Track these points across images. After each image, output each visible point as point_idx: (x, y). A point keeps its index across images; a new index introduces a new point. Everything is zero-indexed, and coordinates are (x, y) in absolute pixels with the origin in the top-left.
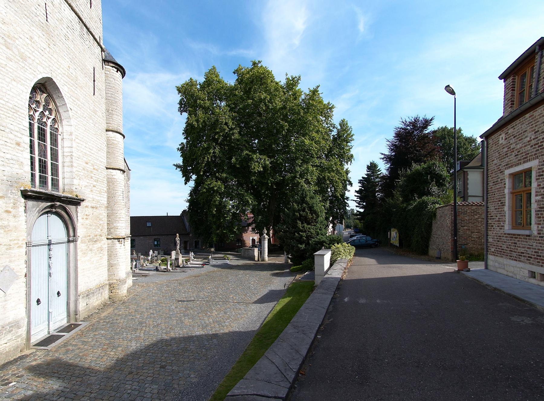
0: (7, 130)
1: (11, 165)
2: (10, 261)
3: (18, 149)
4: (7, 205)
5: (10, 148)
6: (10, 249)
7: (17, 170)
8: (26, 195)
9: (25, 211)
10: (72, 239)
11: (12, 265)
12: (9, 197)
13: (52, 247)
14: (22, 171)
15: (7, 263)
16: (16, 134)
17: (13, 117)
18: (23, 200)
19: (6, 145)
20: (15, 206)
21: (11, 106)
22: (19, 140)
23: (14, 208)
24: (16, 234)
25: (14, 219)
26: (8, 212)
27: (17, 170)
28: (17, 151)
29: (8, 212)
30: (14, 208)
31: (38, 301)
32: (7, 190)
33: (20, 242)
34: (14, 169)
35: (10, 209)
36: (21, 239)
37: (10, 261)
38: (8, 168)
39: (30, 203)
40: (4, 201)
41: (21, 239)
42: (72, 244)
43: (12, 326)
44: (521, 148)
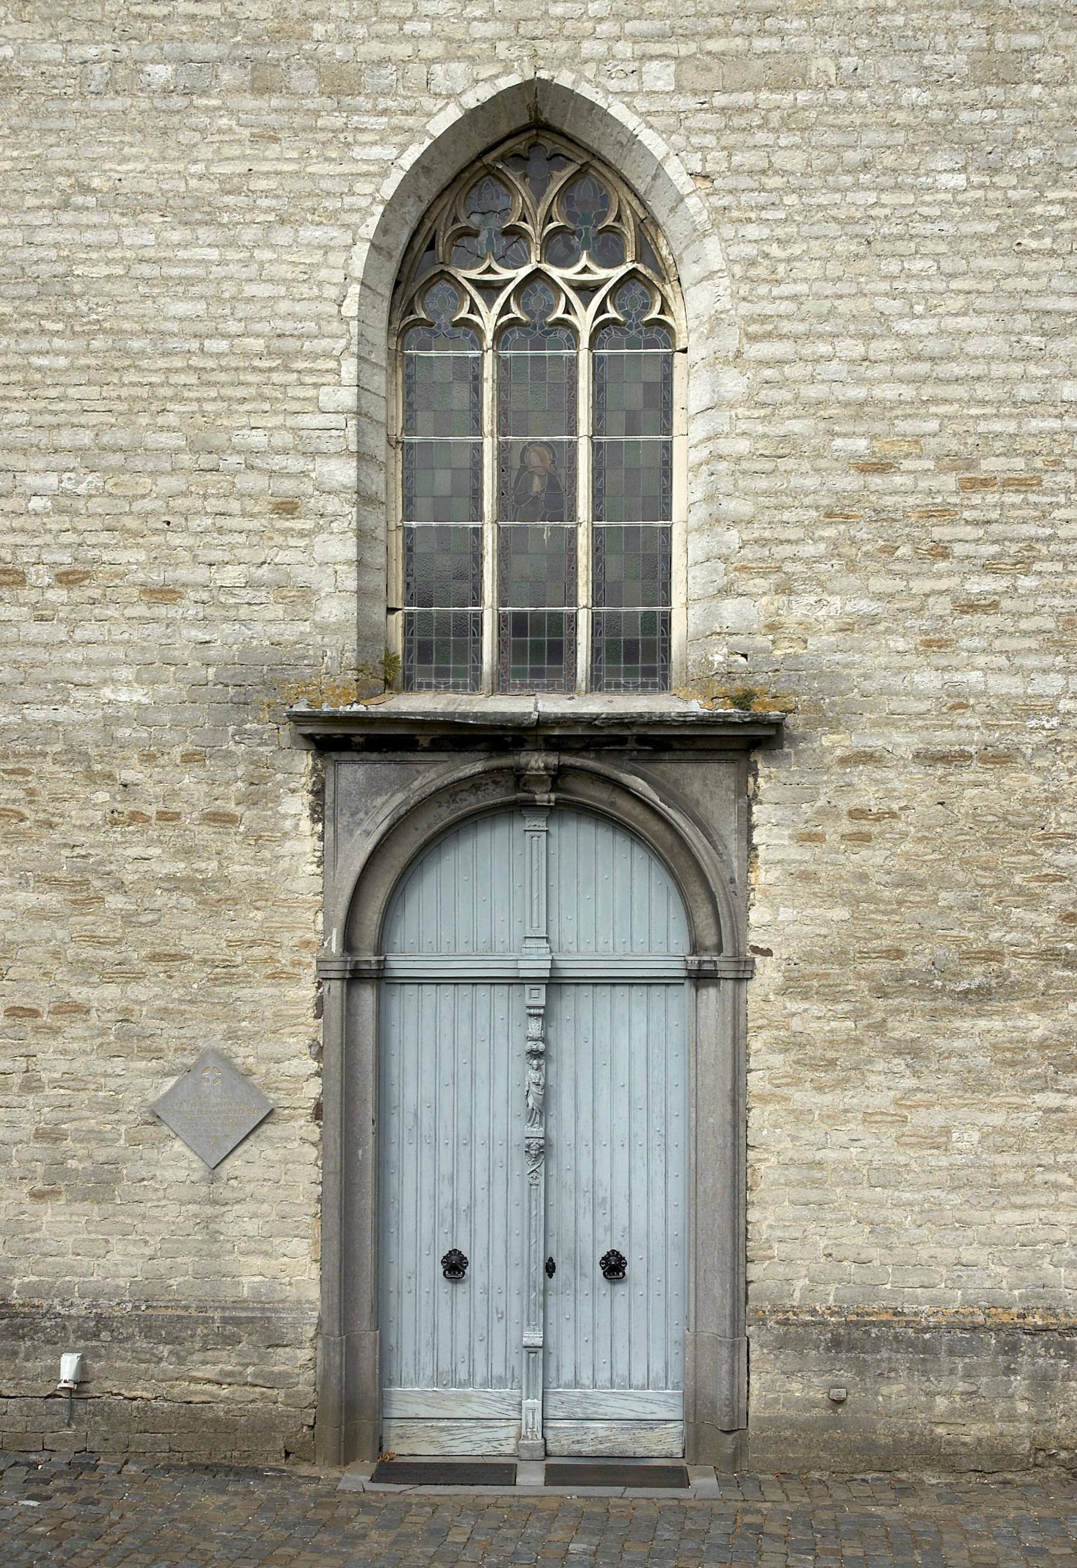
0: (233, 460)
1: (244, 612)
2: (231, 1035)
3: (285, 532)
4: (218, 791)
5: (241, 539)
6: (230, 980)
7: (272, 629)
8: (333, 739)
9: (317, 813)
10: (714, 966)
11: (244, 1055)
12: (229, 754)
13: (576, 1006)
14: (306, 627)
15: (217, 1042)
16: (277, 462)
17: (267, 391)
18: (305, 761)
19: (220, 531)
20: (258, 792)
21: (258, 344)
22: (287, 486)
23: (250, 800)
24: (259, 915)
25: (250, 852)
26: (220, 819)
27: (272, 629)
28: (279, 539)
29: (220, 819)
30: (250, 800)
31: (455, 1266)
32: (220, 725)
33: (284, 958)
34: (258, 627)
35: (232, 807)
36: (289, 939)
37: (231, 1035)
38: (227, 628)
39: (351, 774)
40: (202, 774)
41: (289, 939)
42: (367, 996)
43: (237, 1322)
44: (955, 505)
